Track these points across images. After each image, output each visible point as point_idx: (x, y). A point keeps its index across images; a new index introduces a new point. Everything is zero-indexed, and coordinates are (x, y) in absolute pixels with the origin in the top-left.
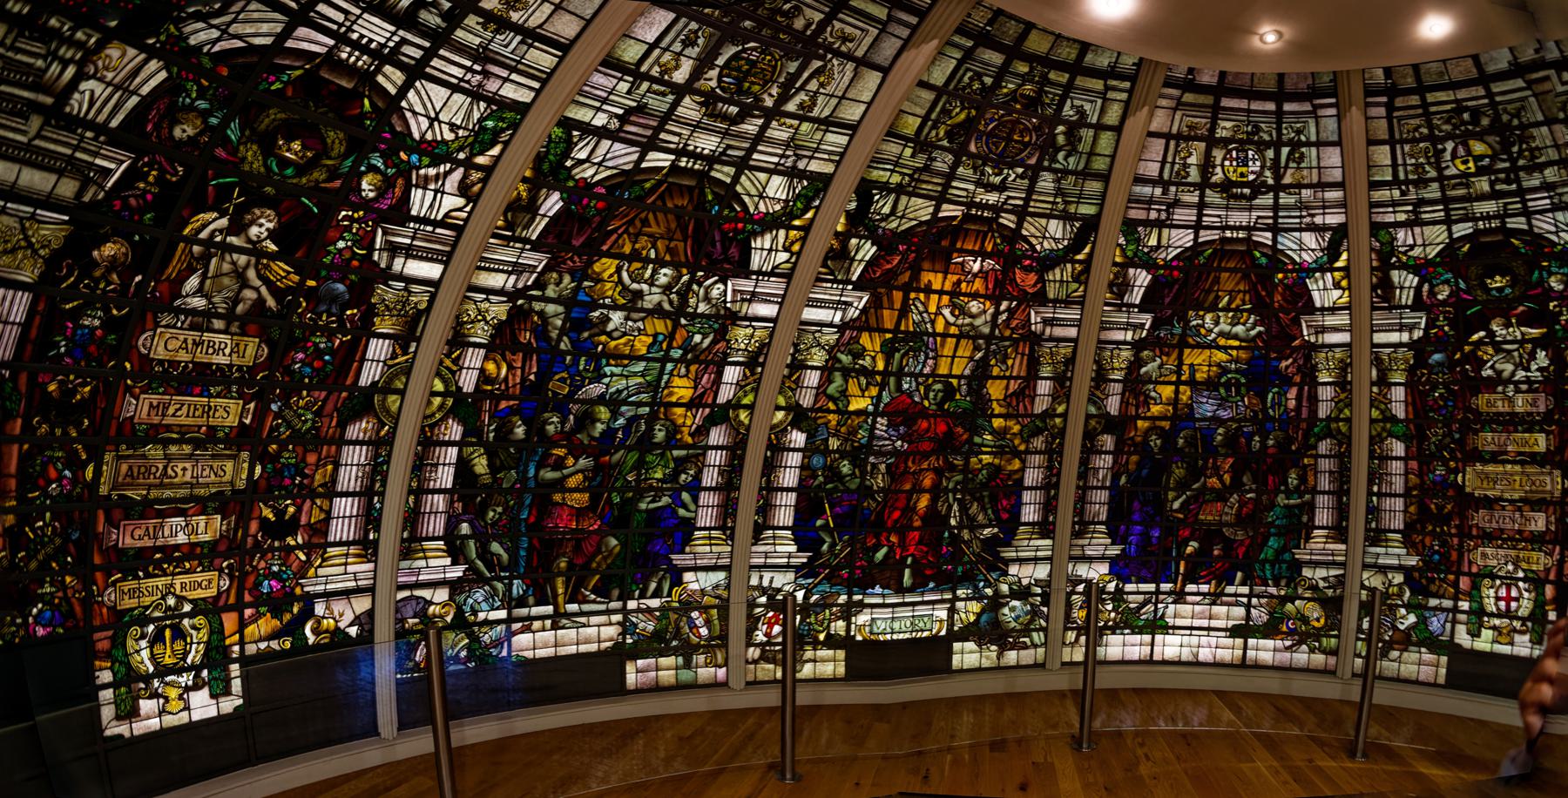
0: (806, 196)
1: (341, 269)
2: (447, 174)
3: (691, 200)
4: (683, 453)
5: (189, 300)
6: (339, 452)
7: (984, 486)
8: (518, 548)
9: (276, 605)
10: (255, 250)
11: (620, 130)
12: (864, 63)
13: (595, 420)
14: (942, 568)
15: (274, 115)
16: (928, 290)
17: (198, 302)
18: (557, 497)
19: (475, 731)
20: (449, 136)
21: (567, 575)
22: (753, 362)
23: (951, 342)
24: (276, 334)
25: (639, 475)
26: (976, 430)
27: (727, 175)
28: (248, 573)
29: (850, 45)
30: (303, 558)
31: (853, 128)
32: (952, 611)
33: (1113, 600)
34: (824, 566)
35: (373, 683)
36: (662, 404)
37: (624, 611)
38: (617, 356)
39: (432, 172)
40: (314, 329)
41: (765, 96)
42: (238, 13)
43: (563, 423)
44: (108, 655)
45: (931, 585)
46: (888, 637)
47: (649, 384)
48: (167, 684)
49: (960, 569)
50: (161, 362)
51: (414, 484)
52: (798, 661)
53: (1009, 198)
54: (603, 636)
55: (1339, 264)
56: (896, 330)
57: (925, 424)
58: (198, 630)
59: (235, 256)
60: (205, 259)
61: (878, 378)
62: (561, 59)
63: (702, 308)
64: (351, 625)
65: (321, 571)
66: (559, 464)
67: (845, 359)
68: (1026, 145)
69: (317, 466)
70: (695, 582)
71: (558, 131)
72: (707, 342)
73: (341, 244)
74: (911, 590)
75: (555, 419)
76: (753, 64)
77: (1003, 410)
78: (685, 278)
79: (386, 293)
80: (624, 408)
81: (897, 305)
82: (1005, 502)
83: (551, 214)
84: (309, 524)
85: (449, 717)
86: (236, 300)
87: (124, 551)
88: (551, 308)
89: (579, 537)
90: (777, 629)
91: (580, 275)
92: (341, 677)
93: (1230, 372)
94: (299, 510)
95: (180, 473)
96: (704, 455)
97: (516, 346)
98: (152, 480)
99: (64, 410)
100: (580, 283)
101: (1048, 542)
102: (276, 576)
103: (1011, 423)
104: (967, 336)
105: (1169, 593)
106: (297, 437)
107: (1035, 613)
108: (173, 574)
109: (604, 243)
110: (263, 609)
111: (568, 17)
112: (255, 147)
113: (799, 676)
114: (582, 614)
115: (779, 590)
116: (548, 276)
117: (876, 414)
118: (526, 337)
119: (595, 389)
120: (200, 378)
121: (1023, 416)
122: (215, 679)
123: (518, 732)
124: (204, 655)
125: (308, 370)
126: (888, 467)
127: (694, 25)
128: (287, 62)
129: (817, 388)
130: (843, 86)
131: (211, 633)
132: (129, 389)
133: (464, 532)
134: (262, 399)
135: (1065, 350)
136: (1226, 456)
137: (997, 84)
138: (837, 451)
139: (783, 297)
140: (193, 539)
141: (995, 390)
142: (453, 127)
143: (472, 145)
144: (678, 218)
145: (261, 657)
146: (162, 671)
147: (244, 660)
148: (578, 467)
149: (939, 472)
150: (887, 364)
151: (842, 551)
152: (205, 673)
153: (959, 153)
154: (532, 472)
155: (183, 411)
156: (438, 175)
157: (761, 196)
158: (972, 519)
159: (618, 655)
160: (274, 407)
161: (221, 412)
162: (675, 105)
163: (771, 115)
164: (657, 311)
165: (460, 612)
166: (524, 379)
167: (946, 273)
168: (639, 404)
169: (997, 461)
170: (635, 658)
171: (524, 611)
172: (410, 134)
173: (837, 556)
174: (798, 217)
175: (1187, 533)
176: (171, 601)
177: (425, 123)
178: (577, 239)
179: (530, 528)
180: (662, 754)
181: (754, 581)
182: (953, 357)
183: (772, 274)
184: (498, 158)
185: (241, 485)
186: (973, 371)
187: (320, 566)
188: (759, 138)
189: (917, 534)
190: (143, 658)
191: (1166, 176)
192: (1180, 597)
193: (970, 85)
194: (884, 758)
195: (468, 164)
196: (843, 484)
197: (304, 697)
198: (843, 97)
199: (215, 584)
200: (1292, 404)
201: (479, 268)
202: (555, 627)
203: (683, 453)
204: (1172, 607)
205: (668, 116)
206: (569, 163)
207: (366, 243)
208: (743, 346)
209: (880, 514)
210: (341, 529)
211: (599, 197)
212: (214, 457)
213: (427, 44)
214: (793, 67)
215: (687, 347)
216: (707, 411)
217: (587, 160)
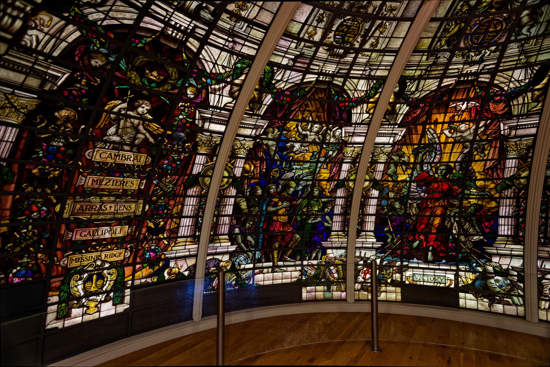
0: (375, 88)
1: (182, 127)
2: (223, 88)
4: (326, 200)
5: (111, 137)
6: (184, 200)
7: (472, 215)
8: (258, 239)
9: (151, 263)
10: (141, 117)
11: (294, 65)
12: (403, 19)
14: (447, 253)
15: (141, 60)
16: (436, 123)
17: (116, 139)
18: (275, 218)
19: (236, 318)
20: (222, 71)
21: (279, 249)
22: (355, 161)
23: (449, 146)
24: (154, 153)
25: (308, 209)
26: (468, 188)
27: (340, 82)
28: (140, 250)
29: (394, 12)
30: (166, 243)
31: (396, 52)
32: (457, 276)
34: (389, 248)
35: (193, 296)
36: (317, 180)
37: (302, 265)
38: (298, 161)
39: (217, 87)
40: (172, 151)
41: (355, 43)
42: (112, 6)
43: (277, 188)
44: (58, 289)
45: (444, 261)
46: (422, 283)
47: (311, 172)
48: (90, 300)
49: (460, 255)
50: (98, 163)
51: (216, 213)
52: (378, 292)
53: (485, 65)
54: (293, 276)
56: (419, 143)
57: (436, 185)
58: (111, 275)
59: (132, 120)
60: (118, 120)
61: (411, 166)
62: (266, 34)
63: (332, 140)
64: (186, 271)
65: (174, 248)
66: (276, 205)
68: (497, 32)
69: (174, 206)
71: (268, 68)
72: (335, 154)
73: (181, 117)
75: (274, 187)
76: (349, 27)
77: (483, 177)
78: (325, 128)
79: (202, 137)
80: (301, 182)
81: (420, 132)
82: (487, 224)
83: (268, 104)
84: (170, 229)
85: (225, 311)
86: (135, 138)
87: (75, 242)
88: (270, 143)
89: (284, 235)
90: (368, 276)
91: (282, 128)
92: (179, 293)
94: (166, 223)
95: (108, 208)
96: (335, 200)
97: (257, 158)
98: (93, 211)
99: (43, 180)
100: (282, 132)
102: (153, 251)
104: (459, 142)
106: (165, 194)
107: (513, 285)
108: (101, 251)
109: (290, 115)
110: (145, 265)
111: (266, 13)
112: (135, 73)
113: (379, 298)
114: (284, 266)
115: (369, 258)
116: (268, 130)
117: (411, 181)
118: (261, 154)
119: (290, 175)
120: (119, 170)
121: (496, 179)
122: (117, 297)
123: (254, 319)
124: (113, 286)
125: (170, 167)
126: (418, 205)
127: (321, 11)
128: (143, 34)
129: (383, 171)
130: (391, 31)
131: (118, 276)
132: (80, 173)
133: (236, 232)
134: (149, 179)
135: (526, 142)
138: (393, 198)
139: (367, 133)
140: (113, 236)
141: (477, 167)
142: (224, 67)
143: (232, 75)
144: (320, 103)
145: (141, 285)
146: (88, 294)
147: (133, 288)
148: (283, 206)
149: (445, 208)
150: (415, 159)
151: (397, 242)
152: (112, 294)
154: (264, 208)
155: (110, 183)
156: (219, 88)
157: (355, 90)
159: (299, 284)
160: (155, 182)
161: (129, 184)
162: (316, 52)
164: (314, 142)
165: (233, 265)
166: (261, 171)
169: (480, 203)
170: (306, 286)
172: (206, 70)
173: (395, 244)
174: (372, 98)
176: (99, 263)
177: (211, 66)
178: (278, 114)
179: (264, 230)
180: (317, 332)
181: (357, 254)
182: (451, 153)
183: (361, 124)
184: (244, 81)
185: (139, 213)
186: (463, 159)
187: (174, 246)
188: (353, 63)
189: (434, 236)
190: (79, 289)
194: (424, 345)
195: (232, 83)
196: (397, 212)
197: (160, 303)
198: (391, 37)
199: (122, 255)
201: (240, 127)
202: (273, 272)
203: (326, 200)
205: (313, 57)
206: (274, 82)
207: (192, 116)
208: (350, 155)
209: (415, 226)
210: (184, 231)
211: (287, 96)
212: (126, 202)
213: (207, 28)
214: (367, 26)
215: (327, 157)
216: (336, 182)
217: (281, 80)
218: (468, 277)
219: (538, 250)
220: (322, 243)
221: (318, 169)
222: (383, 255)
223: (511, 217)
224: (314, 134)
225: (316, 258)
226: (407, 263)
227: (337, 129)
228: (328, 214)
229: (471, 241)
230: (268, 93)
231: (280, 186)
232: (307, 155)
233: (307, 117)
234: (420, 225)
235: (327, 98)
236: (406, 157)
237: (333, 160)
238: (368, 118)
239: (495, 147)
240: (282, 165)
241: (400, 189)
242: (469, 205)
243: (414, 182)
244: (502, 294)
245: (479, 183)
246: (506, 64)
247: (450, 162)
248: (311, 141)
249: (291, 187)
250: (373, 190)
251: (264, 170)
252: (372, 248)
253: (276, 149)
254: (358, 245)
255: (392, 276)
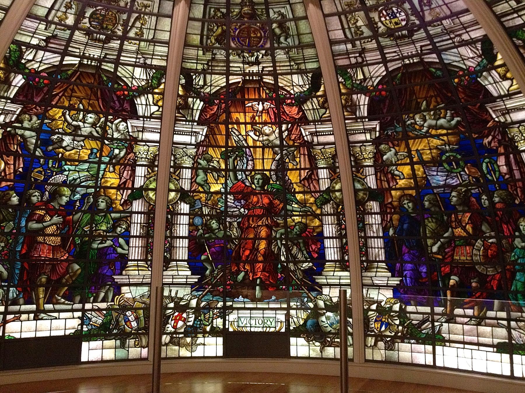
3: (95, 79)
4: (118, 215)
7: (299, 236)
8: (14, 268)
11: (47, 46)
12: (159, 15)
13: (61, 195)
16: (238, 123)
18: (40, 239)
25: (91, 227)
26: (287, 202)
31: (167, 43)
32: (288, 316)
33: (399, 317)
34: (207, 284)
36: (101, 187)
37: (83, 310)
38: (72, 161)
43: (42, 196)
45: (274, 298)
46: (248, 329)
47: (92, 176)
55: (498, 63)
56: (227, 146)
57: (255, 199)
63: (116, 135)
66: (41, 220)
67: (203, 163)
68: (260, 38)
70: (128, 293)
71: (13, 47)
72: (122, 154)
74: (261, 300)
75: (37, 194)
76: (104, 16)
77: (301, 189)
78: (103, 119)
80: (78, 189)
81: (224, 132)
82: (314, 247)
83: (19, 85)
88: (28, 133)
89: (54, 263)
91: (42, 116)
93: (447, 152)
96: (131, 216)
101: (347, 274)
103: (308, 197)
105: (442, 314)
109: (52, 101)
115: (181, 299)
116: (23, 116)
117: (226, 193)
118: (14, 148)
119: (60, 178)
126: (239, 224)
129: (191, 179)
136: (464, 212)
137: (229, 11)
141: (293, 177)
144: (91, 89)
148: (53, 221)
149: (269, 227)
150: (226, 165)
151: (218, 274)
153: (227, 48)
154: (23, 224)
158: (295, 257)
163: (124, 38)
164: (90, 136)
166: (15, 171)
167: (245, 113)
168: (88, 187)
171: (16, 308)
175: (447, 270)
182: (263, 159)
183: (151, 117)
186: (277, 167)
188: (121, 50)
189: (261, 265)
191: (349, 36)
192: (451, 319)
193: (215, 14)
196: (215, 234)
200: (504, 169)
202: (36, 318)
203: (118, 215)
204: (445, 325)
211: (44, 78)
215: (112, 157)
216: (130, 191)
217: (33, 60)
218: (300, 316)
219: (362, 277)
220: (115, 277)
221: (101, 173)
222: (200, 293)
223: (336, 238)
224: (88, 125)
225: (104, 300)
226: (231, 303)
227: (120, 122)
228: (122, 236)
229: (300, 269)
230: (17, 73)
231: (47, 193)
232: (83, 152)
233: (75, 104)
234: (244, 251)
235: (99, 84)
236: (215, 162)
237: (122, 162)
238: (158, 111)
239: (304, 155)
240: (48, 164)
241: (215, 204)
242: (294, 224)
243: (230, 193)
244: (333, 334)
245: (299, 197)
246: (282, 68)
247: (264, 170)
248: (86, 134)
249: (64, 195)
250: (182, 203)
251: (21, 170)
252: (186, 284)
253: (37, 142)
254: (166, 281)
255: (212, 322)
